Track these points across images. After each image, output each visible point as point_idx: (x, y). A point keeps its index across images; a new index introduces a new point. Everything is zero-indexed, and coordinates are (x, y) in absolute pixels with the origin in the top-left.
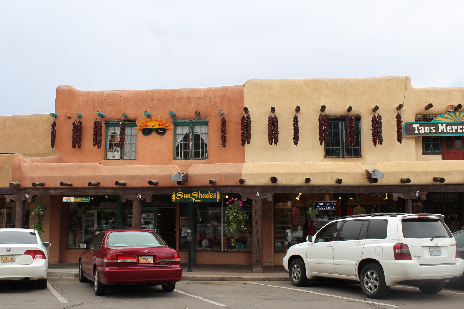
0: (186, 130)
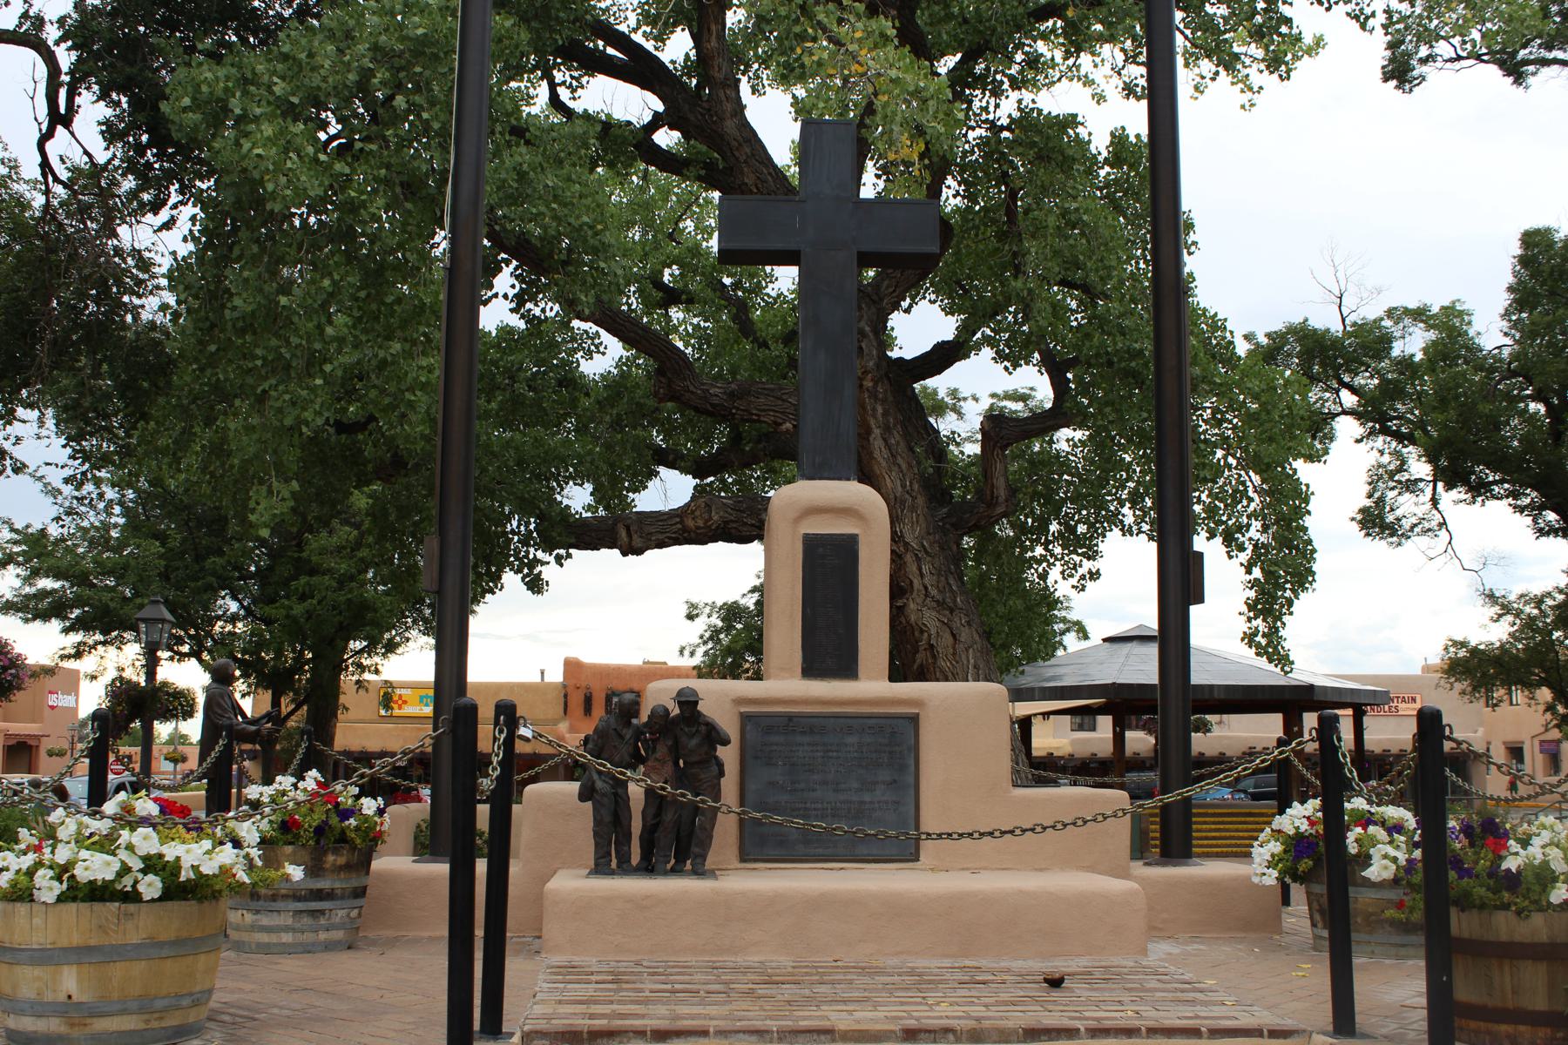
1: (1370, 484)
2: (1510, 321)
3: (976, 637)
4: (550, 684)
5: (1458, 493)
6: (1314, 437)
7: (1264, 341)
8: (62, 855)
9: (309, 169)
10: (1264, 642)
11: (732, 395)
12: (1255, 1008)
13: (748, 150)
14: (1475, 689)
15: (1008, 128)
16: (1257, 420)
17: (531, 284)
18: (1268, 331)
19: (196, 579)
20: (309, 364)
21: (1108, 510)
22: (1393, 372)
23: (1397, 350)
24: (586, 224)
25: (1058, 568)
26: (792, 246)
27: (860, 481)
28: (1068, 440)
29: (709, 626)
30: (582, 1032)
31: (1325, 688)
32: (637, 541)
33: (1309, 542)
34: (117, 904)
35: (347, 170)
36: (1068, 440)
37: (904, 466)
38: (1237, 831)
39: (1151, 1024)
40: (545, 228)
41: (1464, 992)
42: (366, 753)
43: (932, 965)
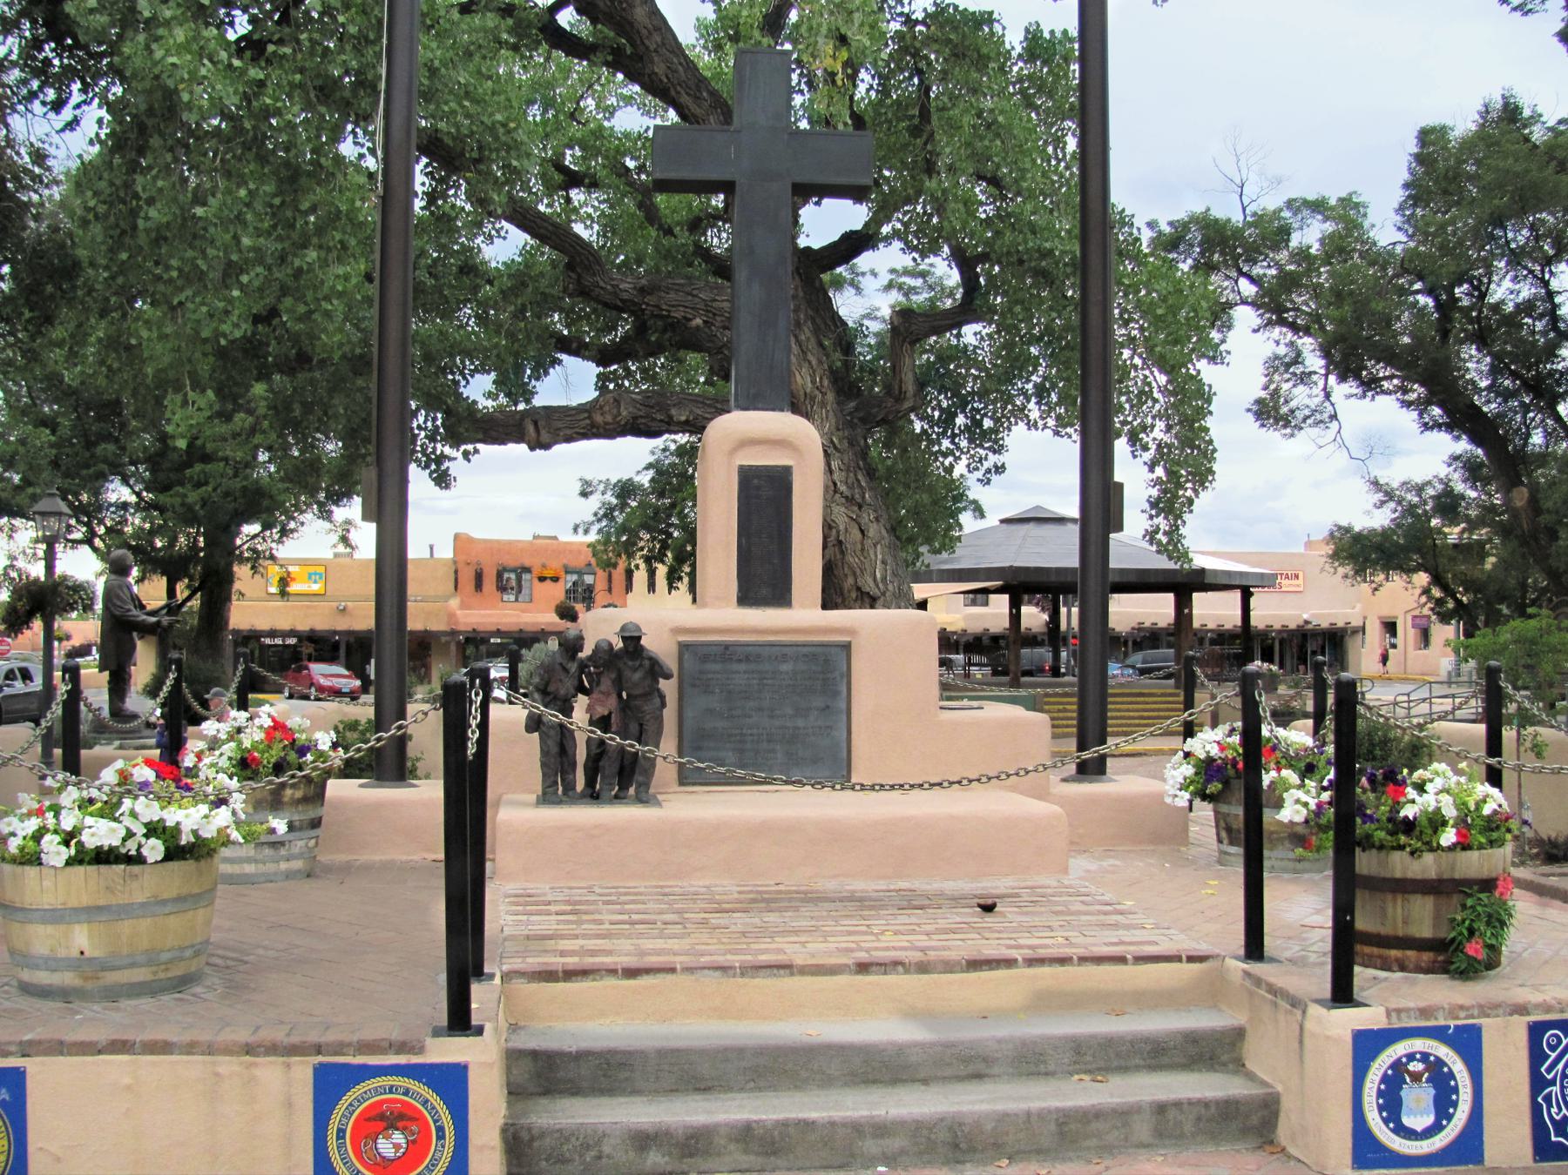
0: (575, 577)
1: (1266, 376)
2: (1404, 216)
3: (884, 532)
4: (440, 560)
5: (1351, 387)
6: (1213, 325)
7: (1167, 229)
8: (68, 822)
9: (225, 78)
10: (1164, 540)
11: (642, 291)
12: (1172, 931)
13: (659, 39)
14: (1357, 573)
15: (923, 22)
16: (1164, 322)
17: (441, 181)
18: (1171, 219)
19: (88, 467)
20: (226, 275)
21: (1014, 405)
22: (1291, 263)
23: (1295, 241)
24: (499, 122)
25: (964, 461)
26: (727, 177)
27: (793, 412)
28: (975, 334)
29: (604, 504)
30: (557, 972)
31: (1215, 572)
32: (545, 437)
33: (1211, 442)
34: (122, 867)
35: (261, 76)
36: (975, 334)
37: (814, 362)
38: (1128, 710)
39: (1081, 952)
40: (458, 126)
41: (1362, 923)
42: (255, 631)
43: (870, 889)
